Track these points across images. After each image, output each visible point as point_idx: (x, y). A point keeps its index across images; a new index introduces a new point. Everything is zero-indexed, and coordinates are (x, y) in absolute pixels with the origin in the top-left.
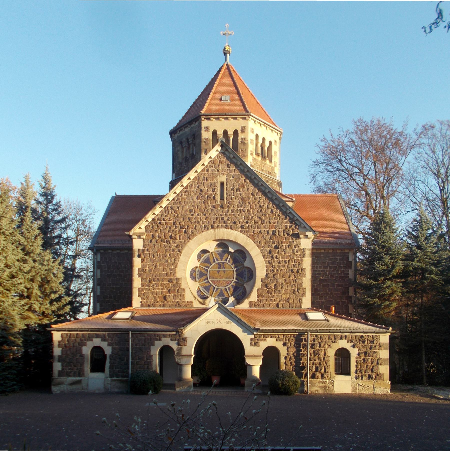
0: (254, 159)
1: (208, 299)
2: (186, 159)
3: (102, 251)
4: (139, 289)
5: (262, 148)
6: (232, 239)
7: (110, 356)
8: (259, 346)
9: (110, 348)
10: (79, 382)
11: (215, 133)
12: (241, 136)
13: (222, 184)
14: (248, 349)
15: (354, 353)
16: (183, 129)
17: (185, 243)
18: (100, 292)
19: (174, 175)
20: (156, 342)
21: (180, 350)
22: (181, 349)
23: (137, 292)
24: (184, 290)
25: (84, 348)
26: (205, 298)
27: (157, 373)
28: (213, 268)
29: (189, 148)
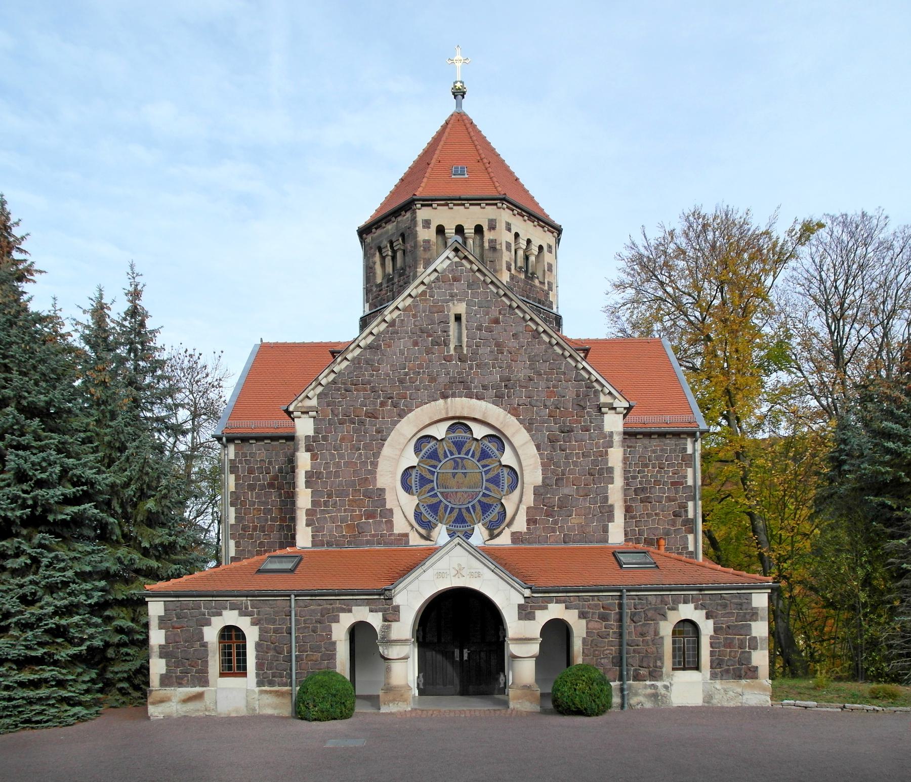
0: (512, 277)
1: (437, 529)
2: (389, 279)
5: (527, 258)
8: (534, 619)
9: (256, 628)
10: (199, 696)
11: (440, 230)
12: (488, 235)
14: (513, 625)
15: (707, 628)
16: (384, 225)
17: (395, 423)
18: (236, 518)
19: (367, 305)
20: (342, 616)
22: (389, 627)
23: (304, 518)
24: (391, 511)
25: (206, 630)
26: (429, 526)
28: (444, 467)
29: (394, 258)
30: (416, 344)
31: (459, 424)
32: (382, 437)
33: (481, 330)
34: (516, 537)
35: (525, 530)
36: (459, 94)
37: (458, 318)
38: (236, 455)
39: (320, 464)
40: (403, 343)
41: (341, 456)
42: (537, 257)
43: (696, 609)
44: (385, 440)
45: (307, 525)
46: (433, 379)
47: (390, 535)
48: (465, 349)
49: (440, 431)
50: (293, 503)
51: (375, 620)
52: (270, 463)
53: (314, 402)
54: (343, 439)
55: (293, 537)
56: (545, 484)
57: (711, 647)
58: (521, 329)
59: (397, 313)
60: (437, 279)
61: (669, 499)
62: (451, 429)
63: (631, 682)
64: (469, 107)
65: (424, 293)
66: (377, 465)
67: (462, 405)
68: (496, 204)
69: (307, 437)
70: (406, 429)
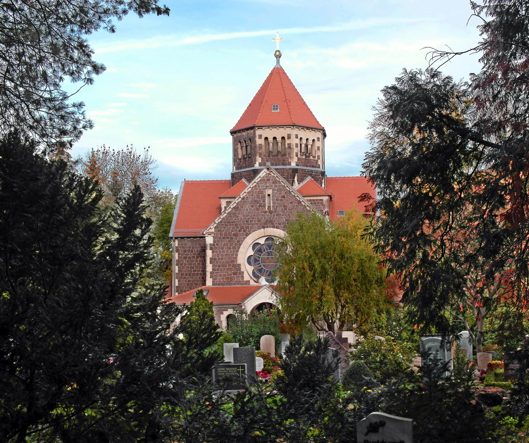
5: (307, 146)
12: (287, 142)
17: (245, 238)
18: (178, 270)
19: (235, 167)
24: (243, 272)
26: (258, 277)
28: (264, 256)
30: (252, 206)
31: (270, 238)
32: (239, 244)
36: (278, 56)
38: (179, 244)
39: (215, 255)
40: (247, 206)
41: (224, 252)
42: (312, 146)
46: (259, 221)
49: (262, 241)
52: (193, 248)
53: (213, 230)
54: (224, 245)
58: (293, 200)
59: (245, 194)
60: (261, 180)
62: (266, 240)
64: (284, 63)
65: (256, 186)
69: (210, 244)
70: (249, 240)
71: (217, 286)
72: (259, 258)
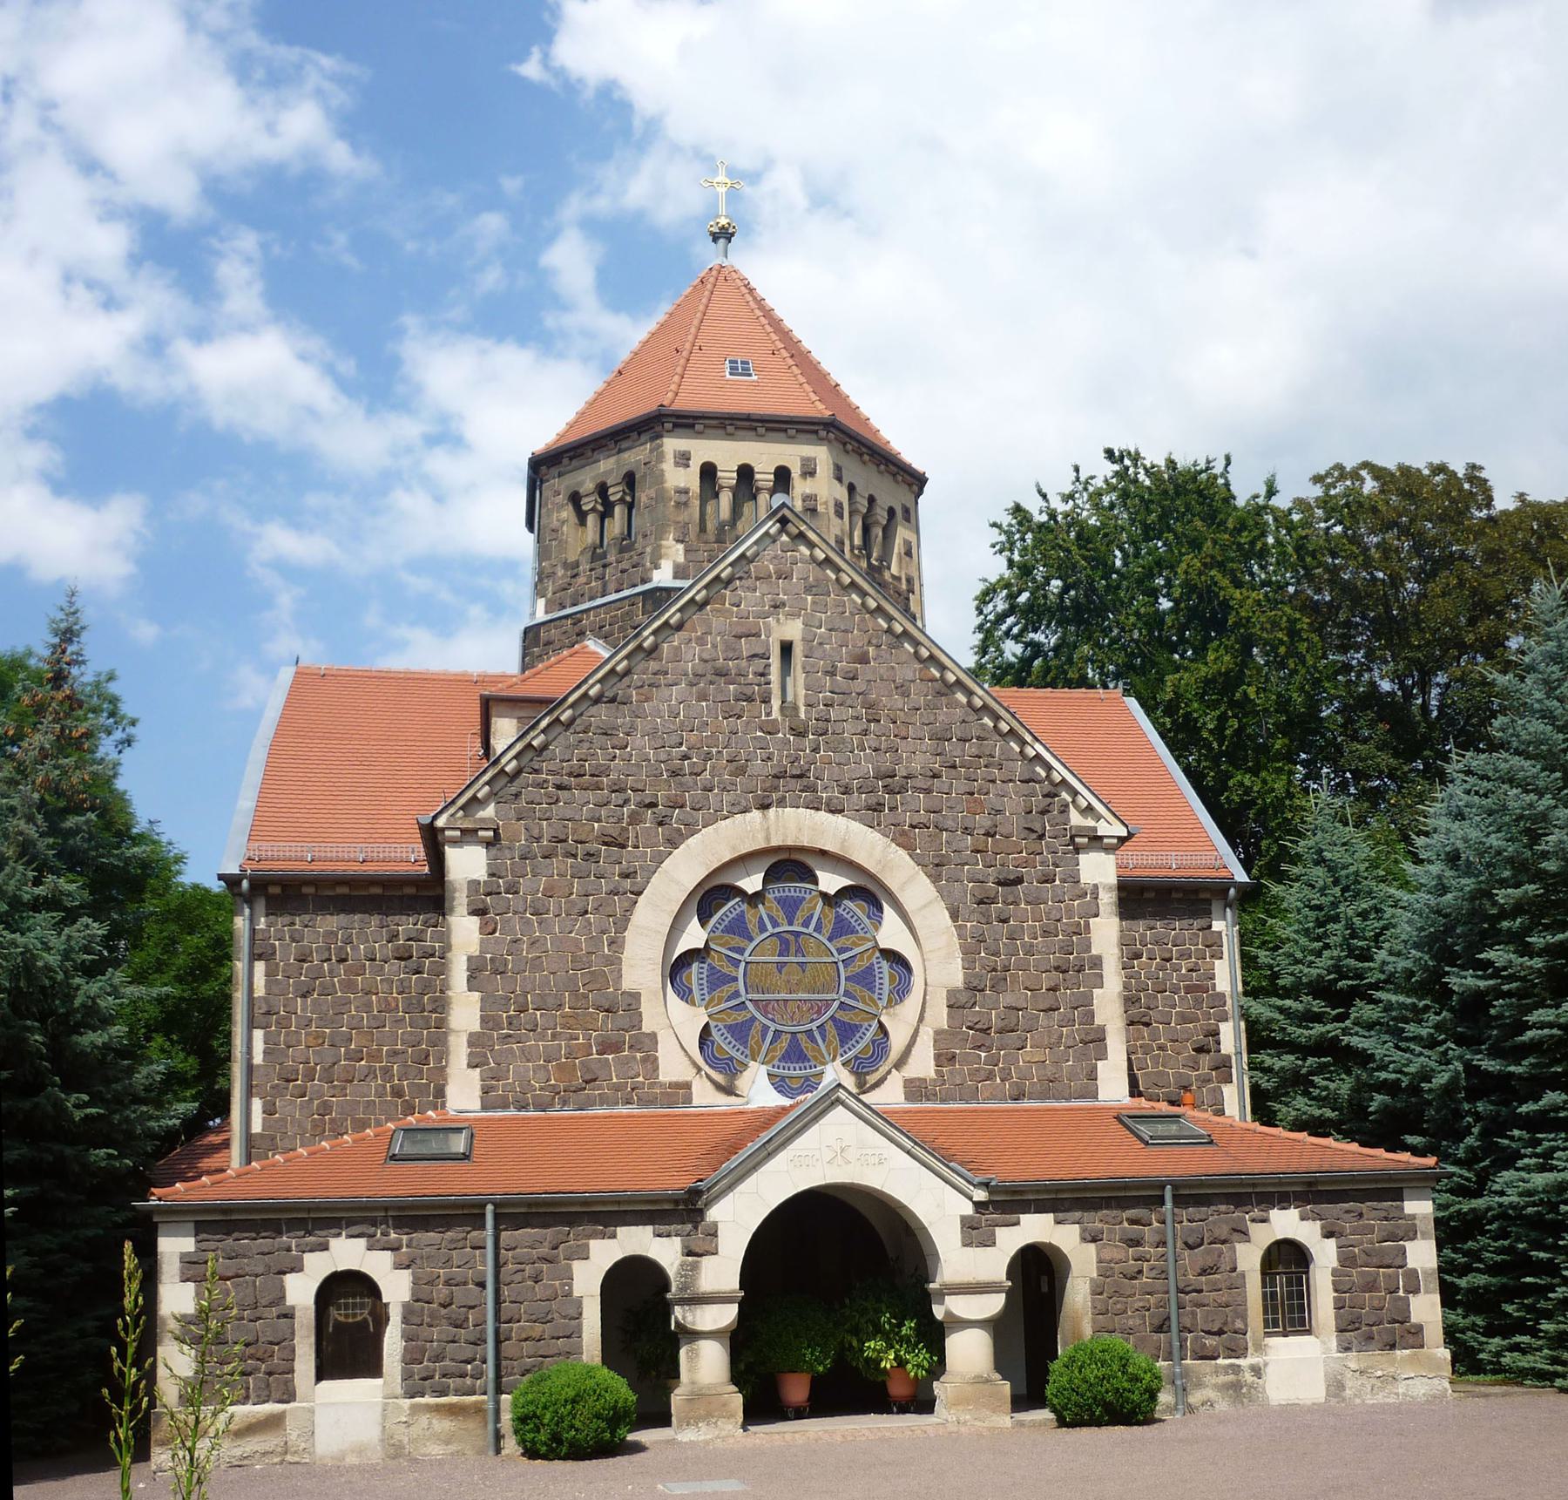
3: (274, 890)
4: (951, 993)
6: (728, 857)
7: (406, 1306)
10: (273, 1423)
11: (708, 472)
13: (786, 649)
14: (956, 1260)
15: (1325, 1255)
17: (660, 860)
21: (691, 1271)
22: (695, 1267)
27: (862, 1336)
33: (832, 674)
34: (915, 1089)
35: (933, 1075)
37: (786, 649)
43: (1302, 1219)
44: (639, 893)
45: (471, 1066)
47: (652, 1086)
48: (802, 709)
50: (441, 1024)
51: (665, 1251)
55: (440, 1093)
56: (972, 988)
57: (1336, 1291)
61: (1184, 1019)
63: (1188, 1361)
66: (622, 946)
67: (796, 825)
68: (816, 432)
69: (473, 885)
71: (511, 1113)
72: (736, 963)
